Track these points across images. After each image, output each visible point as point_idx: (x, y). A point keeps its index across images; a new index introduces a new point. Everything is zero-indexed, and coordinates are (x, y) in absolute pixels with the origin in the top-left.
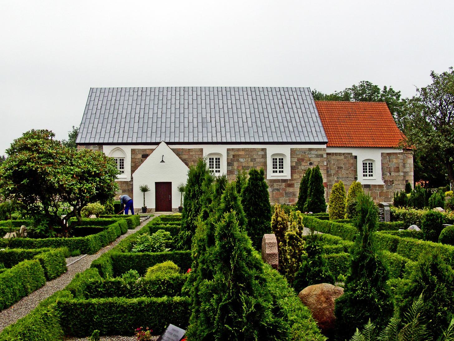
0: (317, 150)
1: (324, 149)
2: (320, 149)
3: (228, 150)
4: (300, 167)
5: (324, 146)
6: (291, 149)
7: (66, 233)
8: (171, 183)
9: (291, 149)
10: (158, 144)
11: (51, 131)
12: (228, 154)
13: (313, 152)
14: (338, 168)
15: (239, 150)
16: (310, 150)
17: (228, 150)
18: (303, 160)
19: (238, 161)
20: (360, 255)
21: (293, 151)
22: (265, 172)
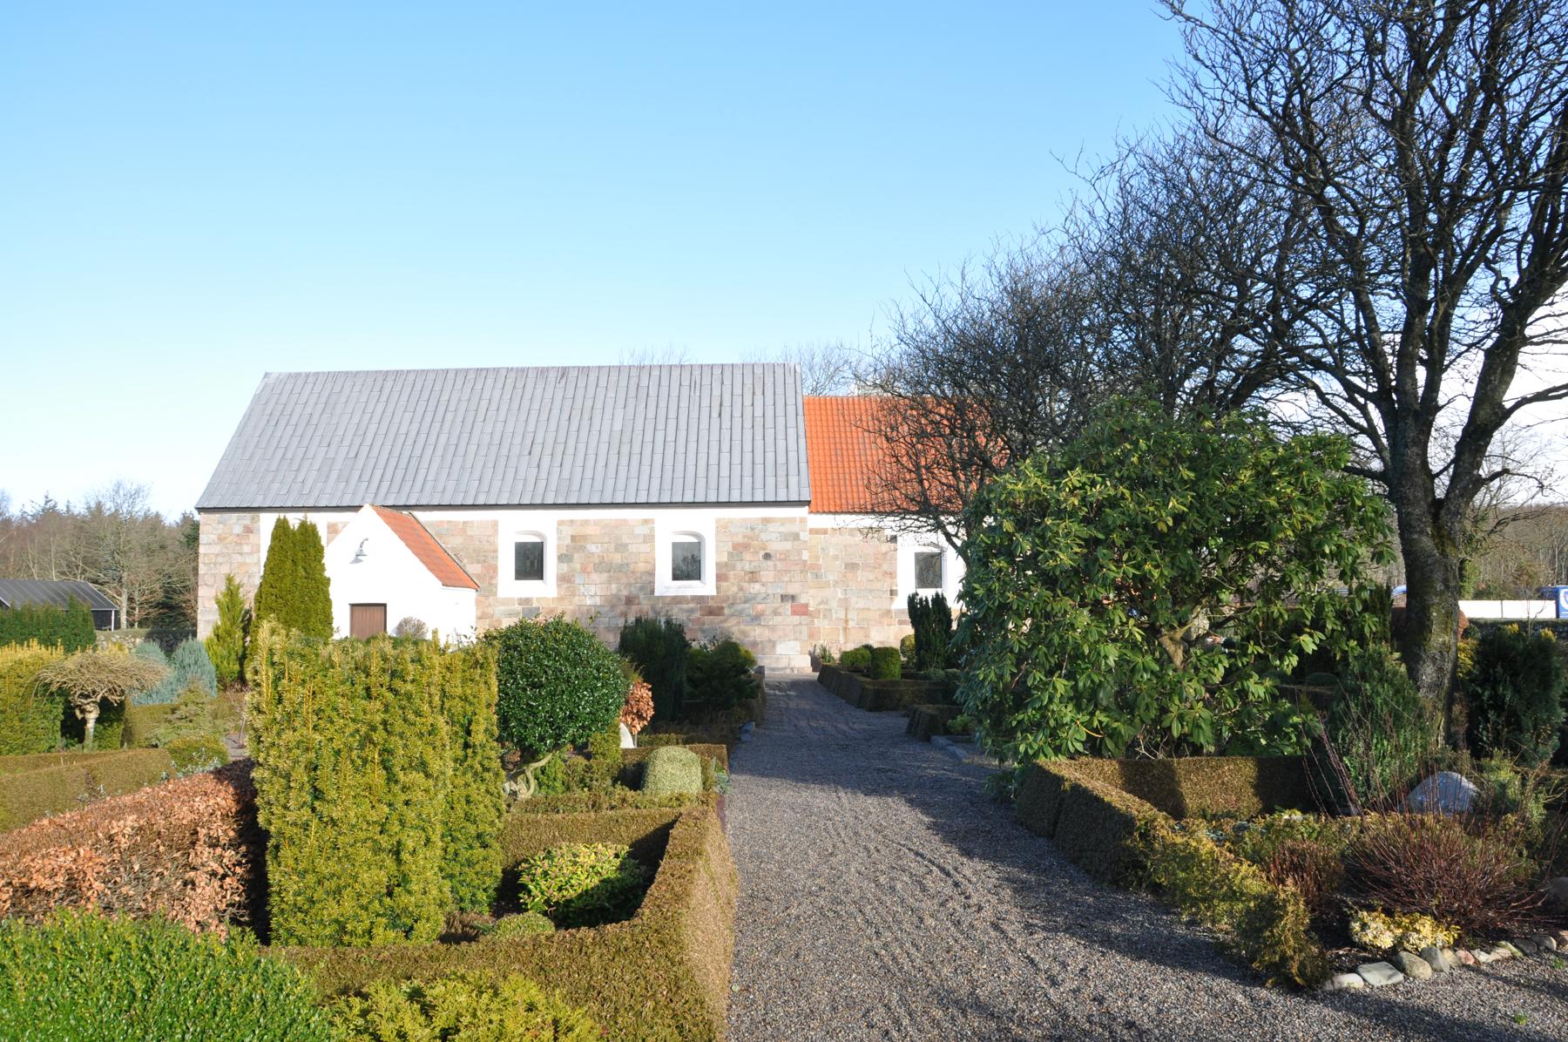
0: (783, 521)
1: (803, 520)
2: (792, 520)
3: (561, 523)
4: (739, 566)
5: (803, 511)
6: (718, 521)
7: (1448, 186)
8: (541, 578)
9: (718, 521)
10: (357, 508)
11: (119, 485)
12: (559, 531)
13: (771, 527)
14: (847, 565)
15: (585, 523)
16: (766, 521)
17: (561, 523)
18: (746, 547)
19: (583, 548)
20: (1328, 987)
21: (722, 528)
22: (1137, 921)
